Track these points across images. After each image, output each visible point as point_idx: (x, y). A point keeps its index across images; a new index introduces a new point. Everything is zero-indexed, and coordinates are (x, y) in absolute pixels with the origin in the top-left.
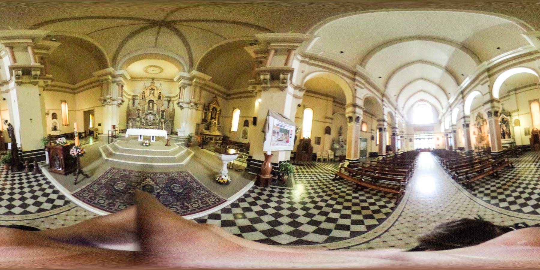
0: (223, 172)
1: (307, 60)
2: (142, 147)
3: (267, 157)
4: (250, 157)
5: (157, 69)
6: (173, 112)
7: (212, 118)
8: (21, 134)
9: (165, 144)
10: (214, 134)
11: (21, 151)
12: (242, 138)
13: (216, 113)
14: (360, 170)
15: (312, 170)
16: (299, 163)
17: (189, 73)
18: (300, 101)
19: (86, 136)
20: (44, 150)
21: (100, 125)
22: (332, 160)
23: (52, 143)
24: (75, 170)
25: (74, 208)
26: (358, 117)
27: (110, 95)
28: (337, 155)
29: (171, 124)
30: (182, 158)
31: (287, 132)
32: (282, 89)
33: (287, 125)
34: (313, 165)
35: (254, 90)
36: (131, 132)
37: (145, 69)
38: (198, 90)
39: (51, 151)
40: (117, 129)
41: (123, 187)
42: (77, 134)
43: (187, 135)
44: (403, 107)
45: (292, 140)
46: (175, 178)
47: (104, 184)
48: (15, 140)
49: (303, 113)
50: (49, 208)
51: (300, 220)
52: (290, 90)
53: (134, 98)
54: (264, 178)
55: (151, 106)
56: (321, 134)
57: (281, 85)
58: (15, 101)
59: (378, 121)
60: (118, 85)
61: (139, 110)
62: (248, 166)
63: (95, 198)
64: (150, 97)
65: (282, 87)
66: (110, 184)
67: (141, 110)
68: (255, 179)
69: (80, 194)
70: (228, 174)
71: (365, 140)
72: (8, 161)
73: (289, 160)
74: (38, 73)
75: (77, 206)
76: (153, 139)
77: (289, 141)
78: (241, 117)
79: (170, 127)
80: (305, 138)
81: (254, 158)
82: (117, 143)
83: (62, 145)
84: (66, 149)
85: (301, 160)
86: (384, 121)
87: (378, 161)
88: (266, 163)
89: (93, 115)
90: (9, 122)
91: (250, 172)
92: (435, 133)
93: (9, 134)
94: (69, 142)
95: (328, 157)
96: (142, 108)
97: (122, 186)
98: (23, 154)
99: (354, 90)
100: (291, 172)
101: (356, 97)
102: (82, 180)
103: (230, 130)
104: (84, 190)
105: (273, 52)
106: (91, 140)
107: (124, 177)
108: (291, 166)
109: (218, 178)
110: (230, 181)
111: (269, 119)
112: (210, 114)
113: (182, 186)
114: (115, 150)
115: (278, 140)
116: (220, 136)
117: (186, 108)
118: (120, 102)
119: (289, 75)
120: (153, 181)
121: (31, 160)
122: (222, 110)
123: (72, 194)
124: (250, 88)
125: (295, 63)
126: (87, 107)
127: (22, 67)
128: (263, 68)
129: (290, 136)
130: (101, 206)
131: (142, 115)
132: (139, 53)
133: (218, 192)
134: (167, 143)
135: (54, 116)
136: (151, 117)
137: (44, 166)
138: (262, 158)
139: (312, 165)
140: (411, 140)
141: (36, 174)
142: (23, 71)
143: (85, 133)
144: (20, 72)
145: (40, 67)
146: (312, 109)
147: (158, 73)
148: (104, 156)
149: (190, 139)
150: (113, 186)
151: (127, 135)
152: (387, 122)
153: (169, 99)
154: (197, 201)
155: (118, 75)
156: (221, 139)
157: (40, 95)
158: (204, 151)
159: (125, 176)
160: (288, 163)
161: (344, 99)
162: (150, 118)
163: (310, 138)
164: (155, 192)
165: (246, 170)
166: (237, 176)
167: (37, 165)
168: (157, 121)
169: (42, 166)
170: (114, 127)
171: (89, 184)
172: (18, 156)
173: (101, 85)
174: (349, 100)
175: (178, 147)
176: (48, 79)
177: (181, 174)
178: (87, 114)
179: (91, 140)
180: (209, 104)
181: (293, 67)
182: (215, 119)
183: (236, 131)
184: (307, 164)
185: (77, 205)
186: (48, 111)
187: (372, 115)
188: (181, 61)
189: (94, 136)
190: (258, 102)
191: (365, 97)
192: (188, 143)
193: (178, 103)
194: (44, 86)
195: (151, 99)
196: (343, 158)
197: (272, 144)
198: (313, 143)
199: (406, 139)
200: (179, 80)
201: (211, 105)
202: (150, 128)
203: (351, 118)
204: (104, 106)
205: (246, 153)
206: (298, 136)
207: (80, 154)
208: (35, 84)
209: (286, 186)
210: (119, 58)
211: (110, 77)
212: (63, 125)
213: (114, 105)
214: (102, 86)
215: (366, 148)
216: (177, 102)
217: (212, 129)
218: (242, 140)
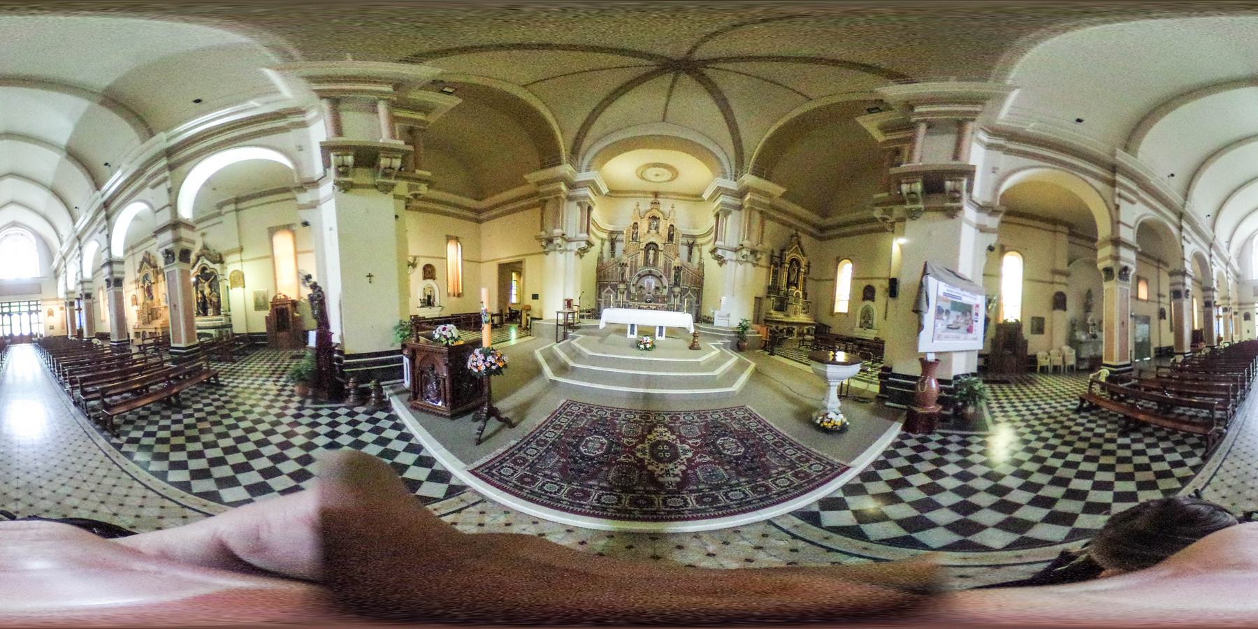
0: (829, 405)
1: (1001, 142)
2: (635, 351)
3: (927, 366)
4: (888, 369)
5: (665, 171)
6: (701, 270)
7: (789, 284)
8: (343, 309)
9: (687, 345)
10: (796, 321)
11: (341, 352)
12: (861, 327)
13: (799, 271)
14: (1134, 386)
15: (1028, 392)
16: (998, 378)
17: (735, 180)
18: (992, 239)
19: (501, 323)
20: (400, 352)
21: (535, 297)
22: (1072, 367)
23: (421, 338)
24: (478, 407)
25: (474, 504)
26: (1126, 269)
27: (562, 228)
28: (1083, 356)
30: (730, 377)
31: (966, 310)
32: (952, 213)
33: (967, 293)
34: (1031, 382)
35: (887, 217)
36: (611, 315)
37: (639, 173)
38: (757, 216)
39: (419, 358)
40: (575, 309)
41: (601, 448)
42: (488, 318)
43: (737, 325)
44: (1229, 242)
45: (979, 327)
46: (723, 424)
47: (553, 444)
48: (327, 326)
49: (1000, 264)
50: (441, 496)
51: (1023, 514)
52: (969, 213)
53: (614, 237)
54: (922, 414)
55: (651, 257)
56: (1043, 311)
57: (948, 204)
58: (331, 229)
59: (1171, 274)
60: (579, 204)
61: (623, 265)
62: (883, 390)
63: (534, 480)
64: (649, 235)
65: (951, 208)
66: (570, 444)
68: (903, 418)
69: (490, 469)
70: (840, 408)
71: (1147, 320)
72: (306, 376)
73: (975, 371)
74: (397, 163)
75: (484, 500)
76: (661, 334)
77: (974, 328)
78: (854, 279)
80: (1009, 321)
81: (896, 370)
82: (578, 341)
83: (447, 345)
84: (458, 354)
85: (1002, 372)
86: (1184, 274)
87: (1173, 367)
88: (925, 379)
89: (520, 274)
90: (314, 279)
91: (888, 404)
92: (42, 300)
93: (313, 308)
94: (468, 336)
95: (1064, 363)
96: (632, 262)
97: (598, 445)
98: (345, 361)
99: (1113, 208)
100: (981, 397)
101: (1119, 222)
102: (495, 433)
103: (833, 308)
104: (502, 460)
105: (922, 128)
106: (513, 332)
107: (603, 425)
108: (980, 384)
109: (821, 418)
110: (848, 423)
111: (927, 281)
112: (786, 274)
113: (741, 441)
114: (573, 359)
115: (949, 327)
116: (811, 324)
117: (731, 260)
118: (583, 245)
119: (965, 182)
120: (673, 433)
121: (367, 376)
122: (812, 265)
123: (472, 467)
124: (877, 213)
125: (976, 154)
126: (505, 256)
127: (355, 146)
128: (905, 167)
129: (974, 317)
130: (551, 498)
131: (631, 279)
132: (630, 134)
133: (827, 449)
134: (694, 342)
135: (429, 272)
136: (651, 282)
137: (397, 394)
138: (916, 370)
139: (1028, 382)
140: (1247, 317)
141: (375, 412)
142: (356, 157)
143: (500, 315)
144: (350, 159)
145: (402, 148)
146: (1018, 252)
147: (669, 181)
148: (548, 372)
149: (743, 332)
150: (576, 447)
151: (602, 324)
152: (1191, 276)
153: (691, 241)
154: (784, 472)
155: (579, 182)
156: (812, 332)
157: (396, 217)
158: (776, 361)
159: (603, 421)
160: (974, 379)
161: (1093, 226)
162: (650, 284)
163: (1019, 320)
164: (683, 457)
165: (880, 399)
166: (861, 413)
167: (379, 389)
168: (665, 292)
169: (391, 392)
170: (569, 303)
171: (513, 443)
172: (332, 359)
173: (542, 204)
174: (1104, 230)
175: (718, 351)
176: (420, 180)
177: (734, 413)
178: (508, 270)
179: (513, 332)
180: (783, 250)
181: (971, 163)
182: (796, 285)
183: (846, 311)
184: (1016, 378)
185: (483, 496)
186: (415, 259)
187: (1159, 261)
188: (721, 155)
189: (521, 323)
190: (897, 244)
191: (1139, 223)
192: (739, 342)
193: (713, 251)
194: (408, 195)
196: (1096, 363)
197: (936, 336)
198: (1026, 332)
199: (1236, 313)
200: (713, 198)
201: (787, 252)
202: (649, 308)
203: (1109, 272)
204: (547, 253)
205: (873, 362)
206: (991, 316)
207: (493, 367)
208: (387, 189)
209: (973, 430)
210: (586, 143)
211: (563, 187)
212: (449, 295)
213: (568, 253)
214: (543, 209)
215: (1149, 338)
216: (710, 247)
217: (791, 308)
218: (859, 333)
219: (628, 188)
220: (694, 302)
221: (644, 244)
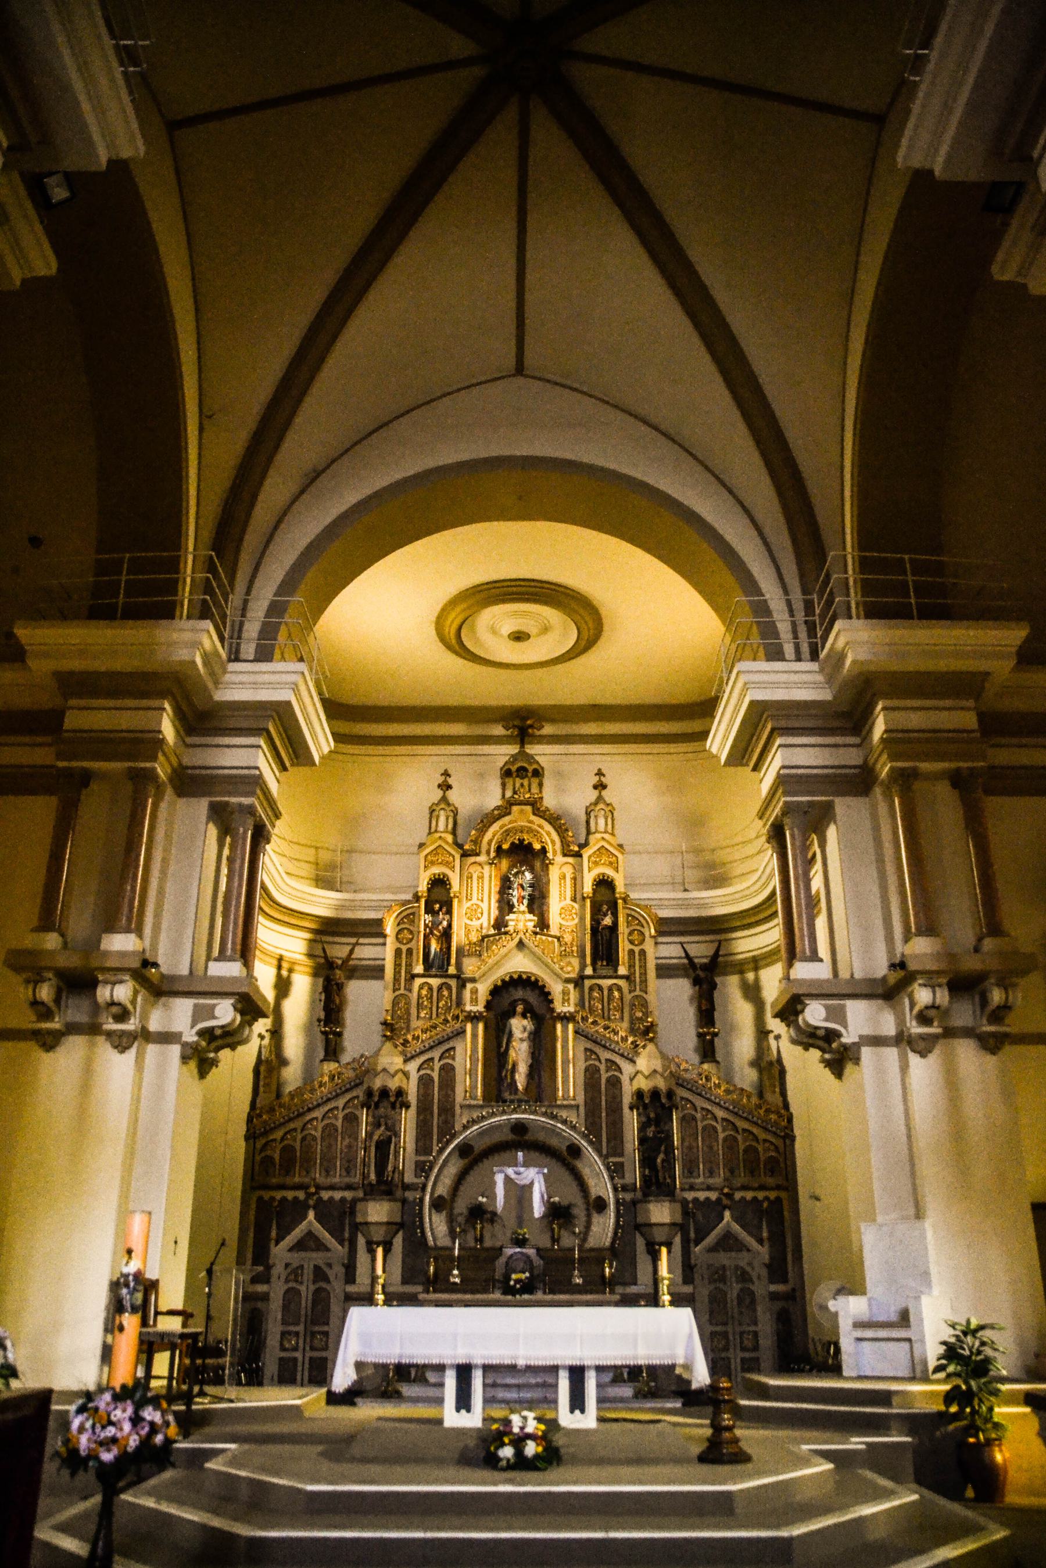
17: (814, 656)
27: (139, 932)
29: (763, 1252)
37: (451, 632)
53: (339, 951)
55: (520, 1053)
60: (221, 815)
67: (412, 1097)
79: (762, 1288)
96: (425, 1082)
117: (877, 1041)
118: (225, 1013)
131: (423, 1169)
153: (700, 949)
162: (520, 1194)
195: (520, 964)
204: (49, 1042)
213: (152, 1049)
219: (383, 699)
220: (759, 1271)
221: (483, 989)
